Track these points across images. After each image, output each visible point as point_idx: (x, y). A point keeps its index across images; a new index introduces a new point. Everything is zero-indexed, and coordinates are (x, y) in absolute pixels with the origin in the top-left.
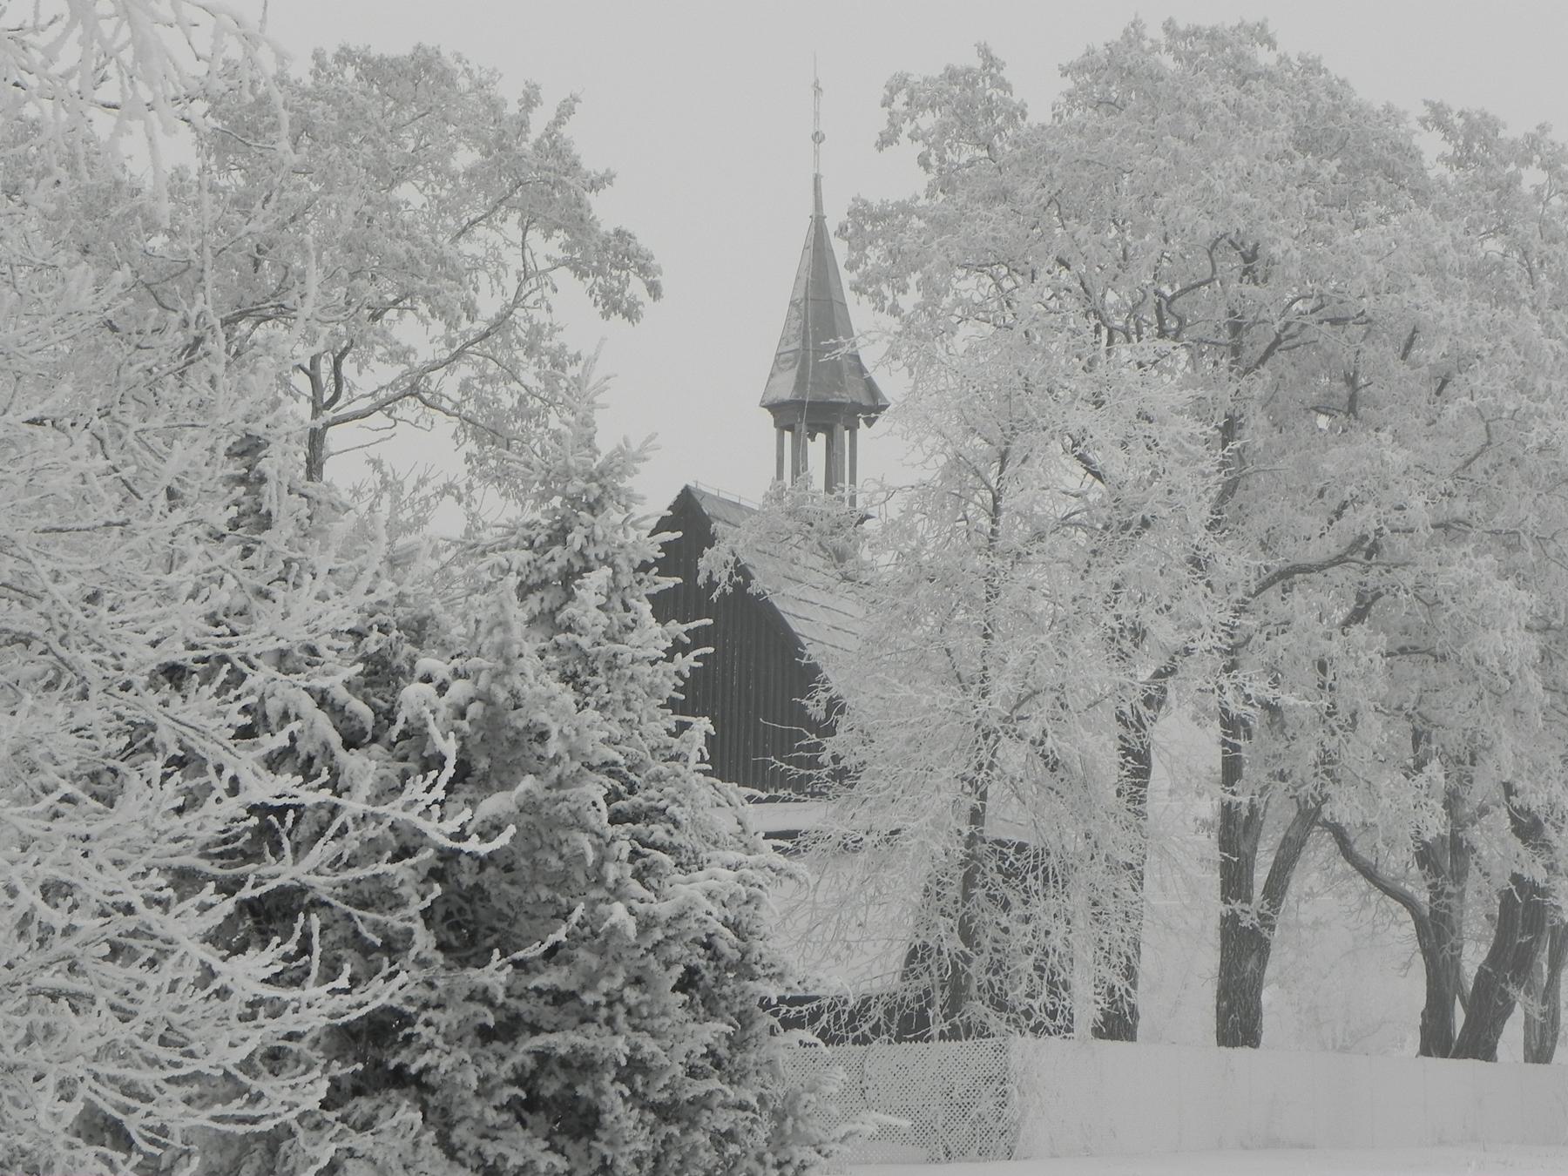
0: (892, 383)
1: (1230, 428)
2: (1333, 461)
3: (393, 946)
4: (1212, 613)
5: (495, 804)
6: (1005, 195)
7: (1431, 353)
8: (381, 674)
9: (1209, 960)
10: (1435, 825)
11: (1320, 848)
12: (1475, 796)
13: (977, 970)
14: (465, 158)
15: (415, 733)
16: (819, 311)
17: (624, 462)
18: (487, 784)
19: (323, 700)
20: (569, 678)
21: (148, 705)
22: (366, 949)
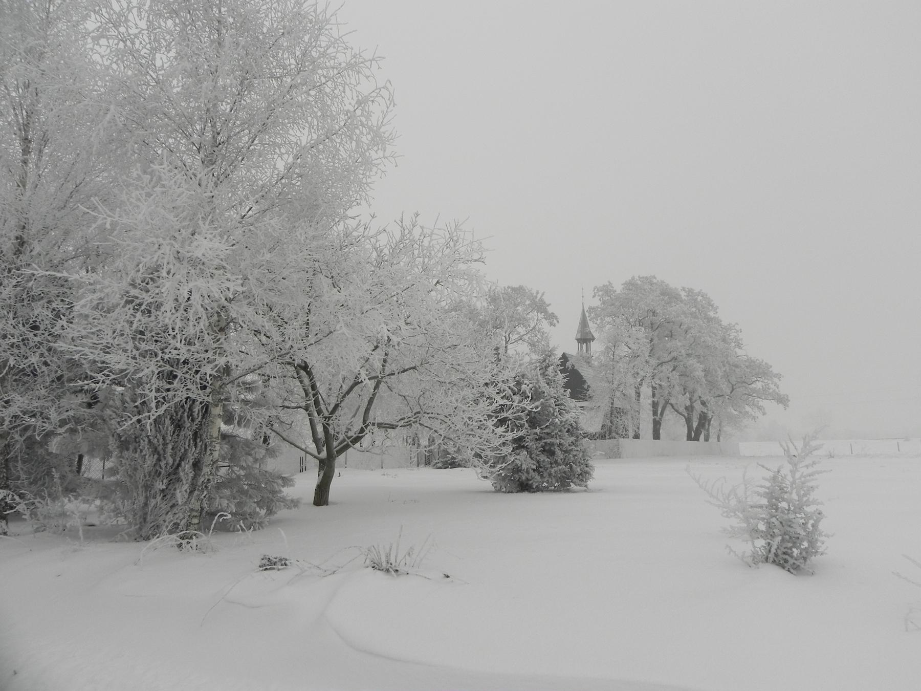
0: (596, 335)
1: (652, 340)
2: (668, 345)
3: (522, 426)
4: (650, 370)
5: (537, 403)
6: (613, 305)
7: (684, 327)
8: (519, 384)
9: (651, 426)
10: (688, 403)
11: (669, 408)
12: (694, 399)
13: (613, 428)
14: (528, 302)
15: (524, 393)
16: (584, 324)
17: (554, 349)
18: (536, 400)
19: (510, 388)
20: (548, 384)
21: (483, 389)
22: (517, 427)
